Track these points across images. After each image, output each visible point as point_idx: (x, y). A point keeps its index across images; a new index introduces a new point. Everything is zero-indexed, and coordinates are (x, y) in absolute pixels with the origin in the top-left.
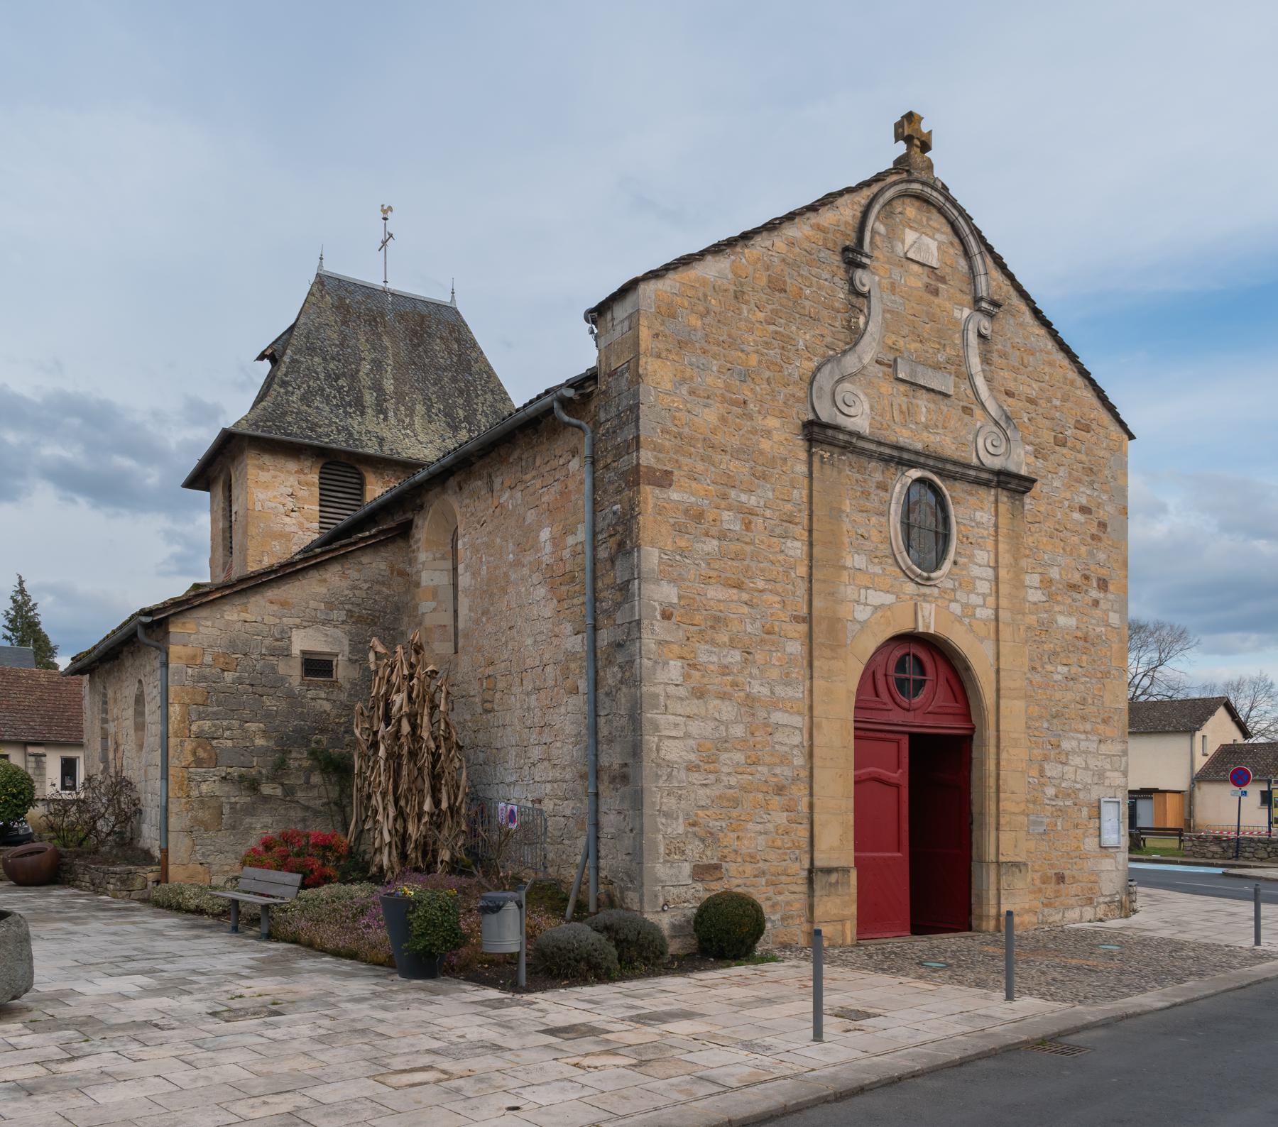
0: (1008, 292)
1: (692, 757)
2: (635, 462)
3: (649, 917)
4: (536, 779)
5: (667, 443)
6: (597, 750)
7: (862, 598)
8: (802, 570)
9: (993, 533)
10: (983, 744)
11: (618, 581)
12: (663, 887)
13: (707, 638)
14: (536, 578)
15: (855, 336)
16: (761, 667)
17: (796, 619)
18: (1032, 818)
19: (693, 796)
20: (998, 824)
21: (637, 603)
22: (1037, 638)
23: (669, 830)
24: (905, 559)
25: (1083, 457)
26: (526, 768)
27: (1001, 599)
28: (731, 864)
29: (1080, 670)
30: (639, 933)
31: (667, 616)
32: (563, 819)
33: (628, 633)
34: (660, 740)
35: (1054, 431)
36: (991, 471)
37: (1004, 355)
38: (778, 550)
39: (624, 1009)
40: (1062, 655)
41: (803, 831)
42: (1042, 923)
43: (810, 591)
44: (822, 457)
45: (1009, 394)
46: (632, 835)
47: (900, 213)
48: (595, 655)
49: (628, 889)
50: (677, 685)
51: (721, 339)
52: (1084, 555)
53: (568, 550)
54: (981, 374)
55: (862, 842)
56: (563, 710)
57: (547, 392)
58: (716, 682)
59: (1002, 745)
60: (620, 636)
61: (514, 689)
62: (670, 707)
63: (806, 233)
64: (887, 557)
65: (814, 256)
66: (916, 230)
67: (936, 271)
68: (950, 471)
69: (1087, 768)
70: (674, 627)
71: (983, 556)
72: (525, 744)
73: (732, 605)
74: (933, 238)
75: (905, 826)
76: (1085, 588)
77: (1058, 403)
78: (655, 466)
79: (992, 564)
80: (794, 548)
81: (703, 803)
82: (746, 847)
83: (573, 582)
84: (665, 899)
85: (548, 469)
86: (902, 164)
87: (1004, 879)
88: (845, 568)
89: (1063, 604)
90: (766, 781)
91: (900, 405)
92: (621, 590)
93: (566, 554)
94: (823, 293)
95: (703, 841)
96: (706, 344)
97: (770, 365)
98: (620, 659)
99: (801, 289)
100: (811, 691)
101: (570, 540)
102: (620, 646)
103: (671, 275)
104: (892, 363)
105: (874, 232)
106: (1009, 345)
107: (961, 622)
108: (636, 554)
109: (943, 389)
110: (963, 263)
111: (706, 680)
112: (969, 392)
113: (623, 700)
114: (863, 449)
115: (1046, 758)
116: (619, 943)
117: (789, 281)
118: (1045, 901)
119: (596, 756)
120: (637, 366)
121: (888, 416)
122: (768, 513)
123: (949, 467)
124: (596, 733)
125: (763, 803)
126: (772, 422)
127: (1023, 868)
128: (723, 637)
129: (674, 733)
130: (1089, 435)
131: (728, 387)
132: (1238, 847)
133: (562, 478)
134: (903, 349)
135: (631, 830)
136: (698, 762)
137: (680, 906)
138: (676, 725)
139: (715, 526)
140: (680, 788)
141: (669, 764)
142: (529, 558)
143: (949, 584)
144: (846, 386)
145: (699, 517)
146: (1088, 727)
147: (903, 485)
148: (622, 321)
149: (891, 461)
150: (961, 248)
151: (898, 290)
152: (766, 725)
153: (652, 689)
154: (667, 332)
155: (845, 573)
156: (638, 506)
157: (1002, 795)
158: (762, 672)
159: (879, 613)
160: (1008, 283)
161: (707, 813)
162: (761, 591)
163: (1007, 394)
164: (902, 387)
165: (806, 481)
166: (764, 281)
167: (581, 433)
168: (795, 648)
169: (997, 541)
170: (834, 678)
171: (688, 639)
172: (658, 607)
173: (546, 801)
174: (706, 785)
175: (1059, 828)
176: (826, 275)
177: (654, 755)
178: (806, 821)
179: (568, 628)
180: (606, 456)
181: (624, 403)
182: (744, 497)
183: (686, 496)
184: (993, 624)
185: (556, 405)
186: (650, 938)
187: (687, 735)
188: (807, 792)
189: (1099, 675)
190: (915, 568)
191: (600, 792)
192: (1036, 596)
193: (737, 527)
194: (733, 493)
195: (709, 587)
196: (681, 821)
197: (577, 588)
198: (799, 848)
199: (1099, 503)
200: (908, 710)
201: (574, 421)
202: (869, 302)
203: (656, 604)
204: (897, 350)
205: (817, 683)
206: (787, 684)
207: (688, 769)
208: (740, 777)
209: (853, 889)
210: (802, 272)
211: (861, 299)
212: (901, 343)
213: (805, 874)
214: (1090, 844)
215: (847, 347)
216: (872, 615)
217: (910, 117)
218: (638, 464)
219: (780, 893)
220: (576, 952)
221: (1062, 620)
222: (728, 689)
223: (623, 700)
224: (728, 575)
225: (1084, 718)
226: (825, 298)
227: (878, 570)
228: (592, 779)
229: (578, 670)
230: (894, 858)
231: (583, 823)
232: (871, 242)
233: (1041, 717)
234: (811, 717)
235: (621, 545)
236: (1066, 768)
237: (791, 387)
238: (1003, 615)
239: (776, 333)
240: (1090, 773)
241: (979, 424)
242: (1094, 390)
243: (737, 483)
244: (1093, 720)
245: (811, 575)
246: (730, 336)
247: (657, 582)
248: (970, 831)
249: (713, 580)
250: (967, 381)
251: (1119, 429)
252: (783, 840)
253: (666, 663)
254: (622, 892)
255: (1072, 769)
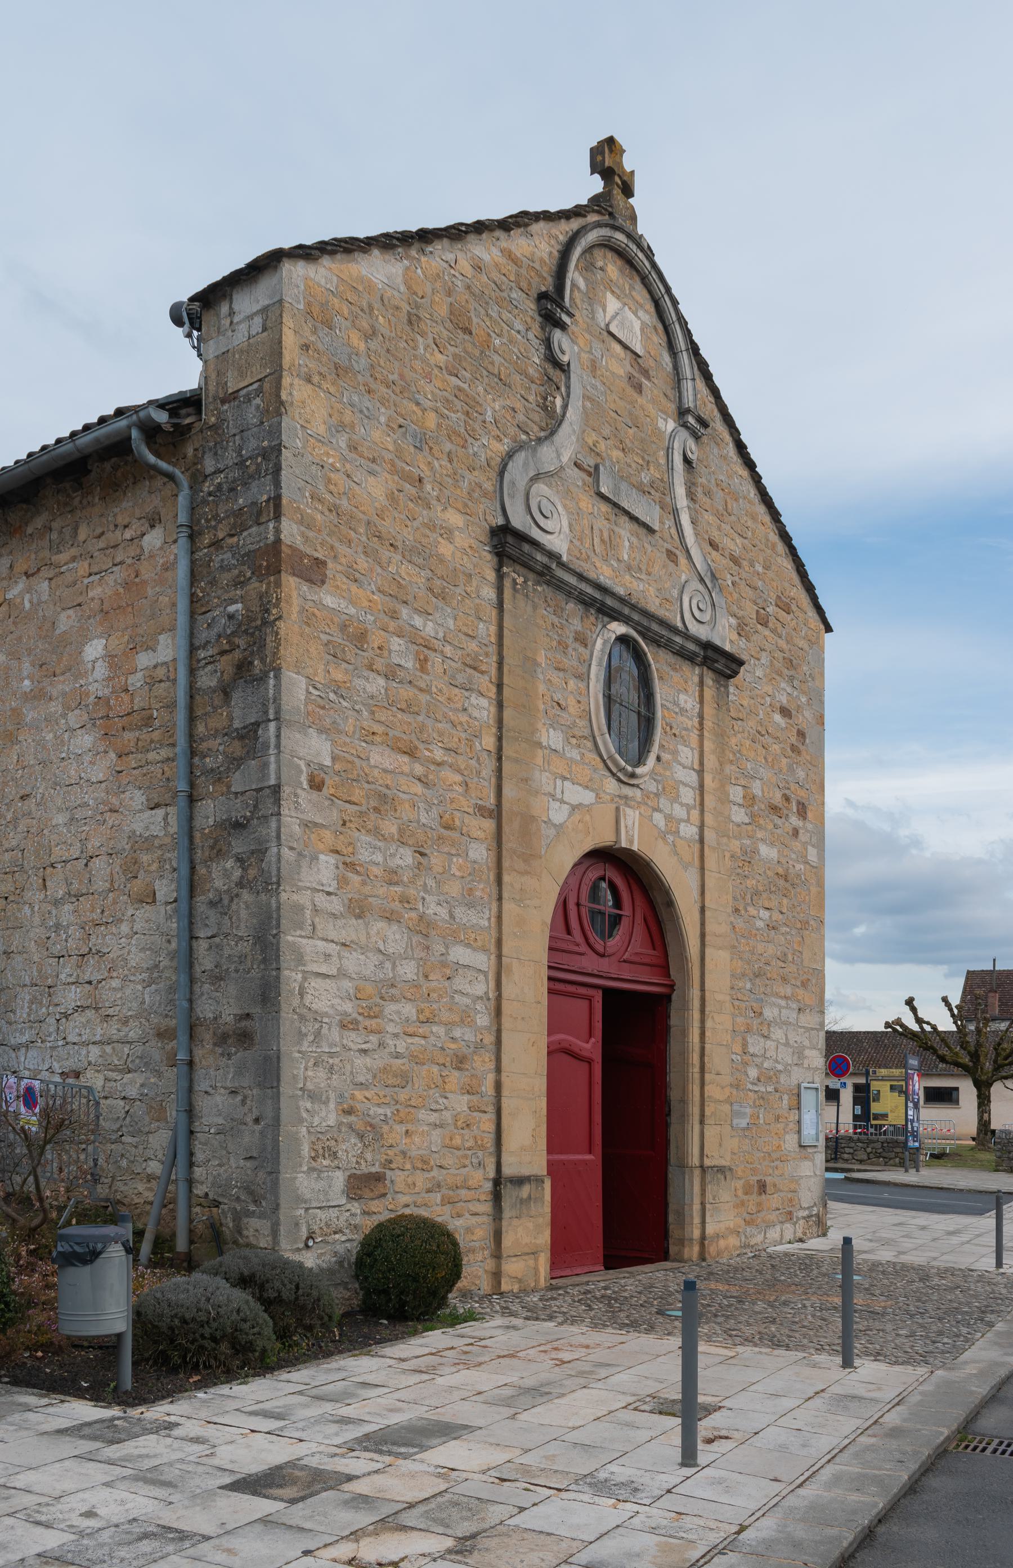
0: (712, 411)
1: (348, 1007)
2: (271, 537)
3: (288, 1255)
4: (70, 1039)
5: (319, 517)
6: (191, 993)
7: (558, 791)
8: (489, 741)
9: (697, 726)
10: (685, 1006)
11: (237, 724)
12: (307, 1209)
13: (370, 825)
14: (74, 718)
15: (553, 423)
16: (438, 876)
17: (481, 811)
18: (736, 1107)
19: (348, 1067)
20: (702, 1115)
21: (272, 759)
22: (740, 871)
23: (316, 1121)
24: (608, 744)
25: (782, 643)
26: (51, 1020)
27: (706, 814)
28: (398, 1172)
29: (781, 916)
30: (297, 1287)
31: (316, 785)
32: (122, 1103)
33: (256, 806)
34: (305, 979)
35: (756, 604)
36: (697, 641)
37: (708, 493)
38: (459, 706)
39: (334, 1428)
40: (765, 895)
41: (486, 1124)
42: (745, 1247)
43: (499, 770)
44: (514, 580)
45: (713, 545)
46: (258, 1128)
47: (601, 269)
48: (191, 838)
49: (250, 1214)
50: (329, 894)
51: (391, 377)
52: (785, 770)
53: (139, 675)
54: (686, 509)
55: (556, 1142)
56: (125, 928)
57: (120, 412)
58: (381, 893)
59: (707, 1009)
60: (239, 810)
61: (28, 895)
62: (319, 927)
63: (496, 259)
64: (586, 738)
65: (505, 294)
66: (618, 298)
67: (640, 360)
68: (656, 633)
69: (787, 1044)
70: (327, 803)
71: (687, 754)
72: (50, 982)
73: (403, 780)
74: (636, 314)
75: (598, 1118)
76: (785, 812)
77: (760, 569)
78: (302, 547)
79: (696, 767)
80: (478, 707)
81: (361, 1079)
82: (417, 1146)
83: (147, 725)
84: (309, 1230)
85: (102, 544)
86: (598, 203)
87: (709, 1188)
88: (539, 745)
89: (765, 829)
90: (442, 1049)
91: (601, 531)
92: (241, 738)
93: (136, 681)
94: (515, 350)
95: (361, 1137)
96: (371, 380)
97: (452, 434)
98: (239, 845)
99: (489, 335)
100: (499, 918)
101: (144, 660)
102: (238, 826)
103: (326, 261)
104: (592, 470)
105: (574, 285)
106: (713, 481)
107: (664, 839)
108: (272, 682)
109: (647, 520)
110: (666, 359)
111: (366, 890)
112: (673, 531)
113: (244, 914)
114: (562, 581)
115: (748, 1030)
116: (268, 1304)
117: (475, 320)
118: (748, 1217)
119: (191, 1001)
120: (278, 386)
121: (587, 543)
122: (448, 650)
123: (655, 627)
124: (191, 965)
125: (440, 1082)
126: (454, 519)
127: (728, 1174)
128: (391, 828)
129: (323, 969)
130: (789, 617)
131: (399, 452)
132: (837, 1146)
133: (129, 561)
134: (604, 454)
135: (257, 1121)
136: (355, 1015)
137: (330, 1239)
138: (328, 956)
139: (380, 656)
140: (331, 1055)
141: (318, 1017)
142: (63, 685)
143: (652, 787)
144: (541, 488)
145: (360, 638)
146: (788, 991)
147: (605, 642)
148: (250, 317)
149: (591, 605)
150: (665, 339)
151: (599, 373)
152: (444, 964)
153: (295, 897)
154: (320, 346)
155: (540, 753)
156: (277, 605)
157: (707, 1076)
158: (438, 883)
159: (577, 817)
160: (712, 399)
161: (367, 1094)
162: (439, 764)
163: (711, 545)
164: (604, 507)
165: (494, 613)
166: (443, 311)
167: (171, 485)
168: (480, 853)
169: (701, 736)
170: (528, 902)
171: (344, 824)
172: (304, 768)
173: (89, 1074)
174: (365, 1051)
175: (762, 1122)
176: (518, 326)
177: (296, 1002)
178: (491, 1109)
179: (137, 798)
180: (215, 528)
181: (253, 443)
182: (418, 621)
183: (343, 604)
184: (697, 846)
185: (135, 433)
186: (315, 1293)
187: (342, 974)
188: (492, 1066)
189: (799, 926)
190: (617, 756)
191: (197, 1059)
192: (739, 815)
193: (409, 664)
194: (405, 612)
195: (373, 748)
196: (332, 1105)
197: (156, 735)
198: (482, 1148)
199: (799, 706)
200: (602, 956)
201: (163, 465)
202: (569, 378)
203: (302, 764)
204: (598, 454)
205: (507, 906)
206: (470, 905)
207: (343, 1026)
208: (410, 1040)
209: (547, 1209)
210: (490, 312)
211: (558, 372)
212: (602, 446)
213: (489, 1186)
214: (790, 1142)
215: (542, 434)
216: (570, 816)
217: (610, 142)
218: (278, 541)
219: (459, 1216)
220: (214, 1325)
221: (764, 850)
222: (397, 906)
223: (244, 914)
224: (397, 734)
225: (784, 979)
226: (518, 357)
227: (574, 754)
228: (183, 1037)
229: (154, 867)
230: (585, 1162)
231: (162, 1109)
232: (571, 298)
233: (744, 975)
234: (499, 957)
235: (243, 667)
236: (769, 1043)
237: (476, 473)
238: (709, 835)
239: (460, 389)
240: (790, 1050)
241: (684, 578)
242: (794, 560)
243: (410, 598)
244: (793, 982)
245: (500, 749)
246: (402, 376)
247: (304, 728)
248: (667, 1126)
249: (378, 739)
250: (672, 516)
251: (817, 617)
252: (463, 1135)
253: (315, 858)
254: (237, 1218)
255: (774, 1044)
